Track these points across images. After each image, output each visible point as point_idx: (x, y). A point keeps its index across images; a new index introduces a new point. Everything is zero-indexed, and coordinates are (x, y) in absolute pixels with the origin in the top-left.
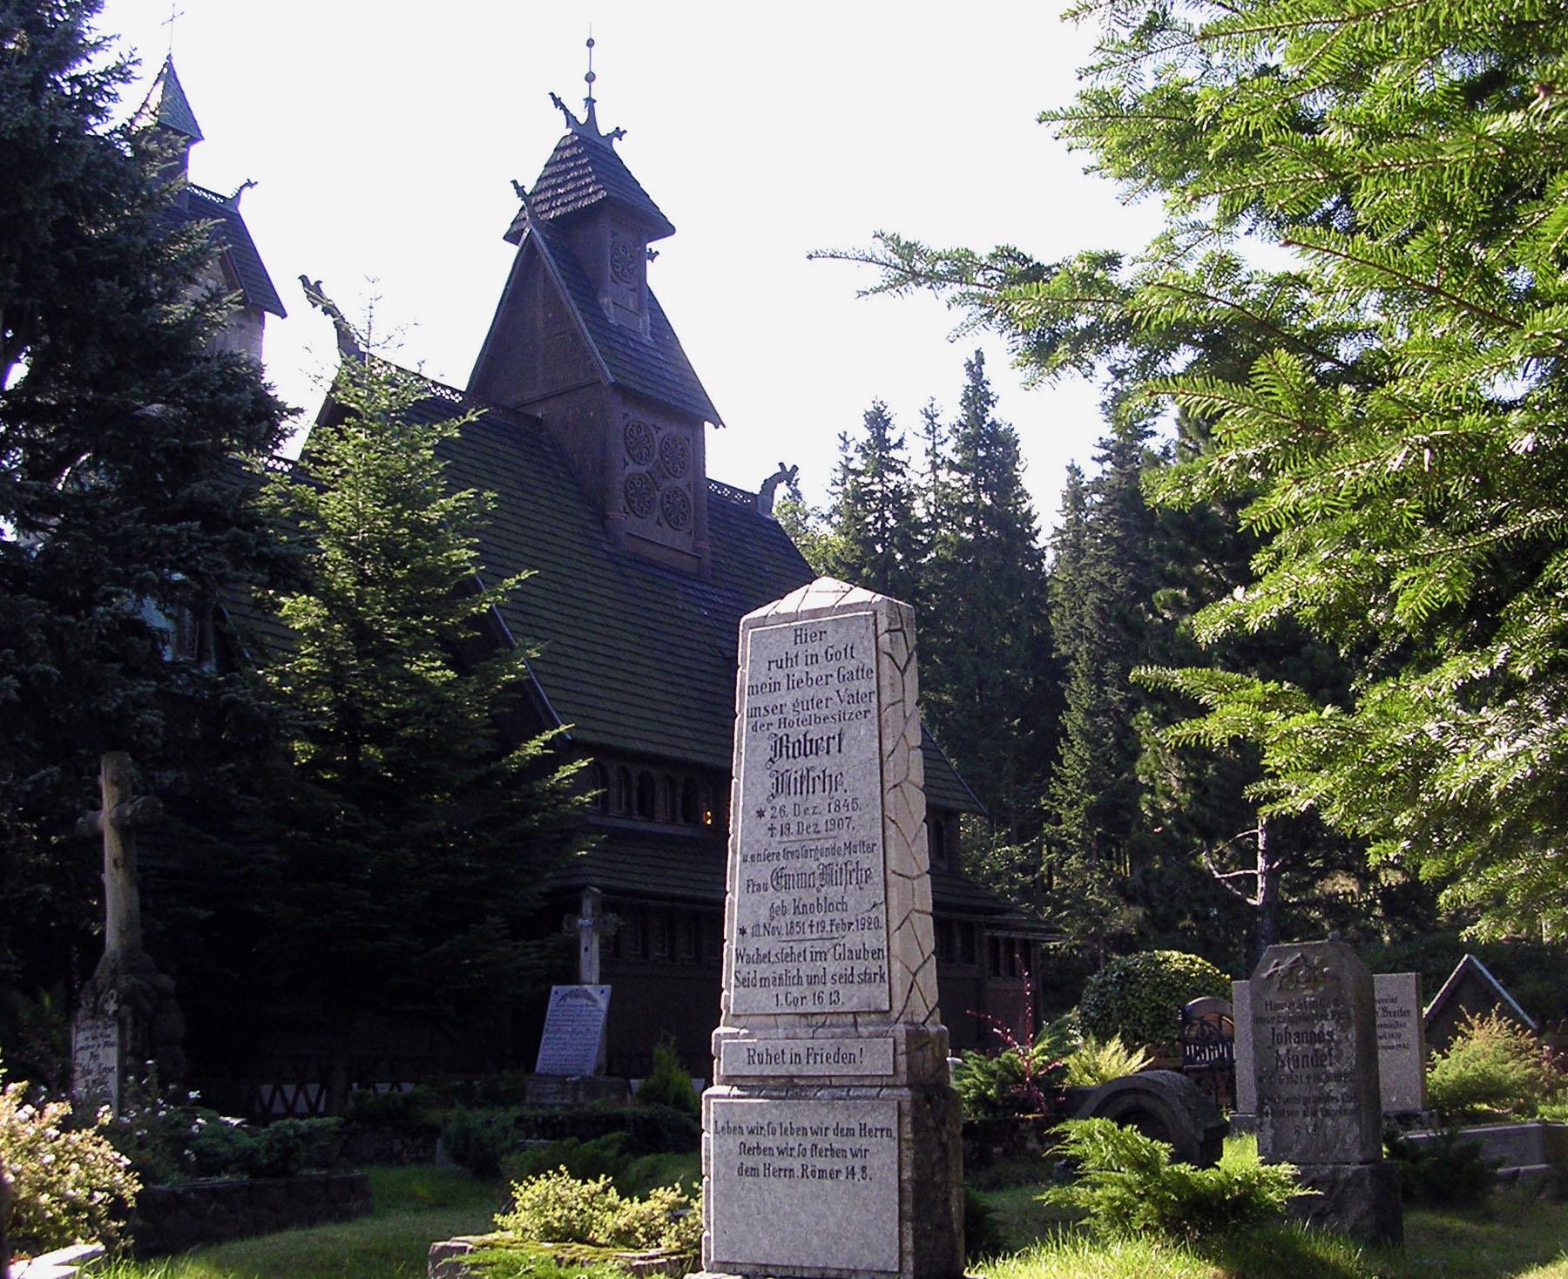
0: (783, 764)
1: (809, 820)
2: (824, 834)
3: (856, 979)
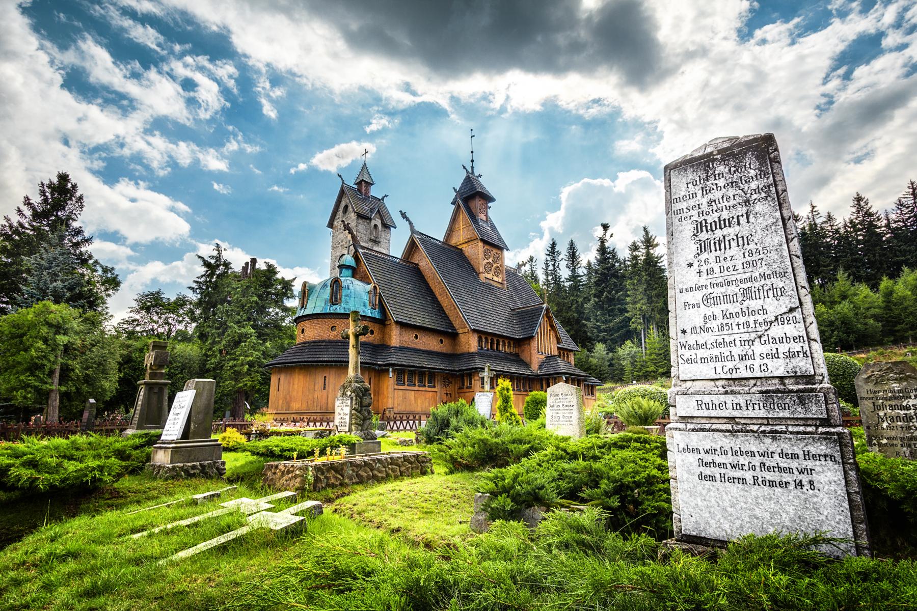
0: (703, 236)
2: (742, 271)
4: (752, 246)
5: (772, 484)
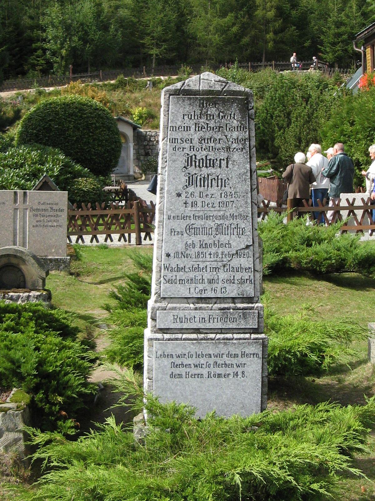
0: (192, 170)
1: (207, 200)
3: (236, 282)
4: (227, 189)
5: (219, 376)
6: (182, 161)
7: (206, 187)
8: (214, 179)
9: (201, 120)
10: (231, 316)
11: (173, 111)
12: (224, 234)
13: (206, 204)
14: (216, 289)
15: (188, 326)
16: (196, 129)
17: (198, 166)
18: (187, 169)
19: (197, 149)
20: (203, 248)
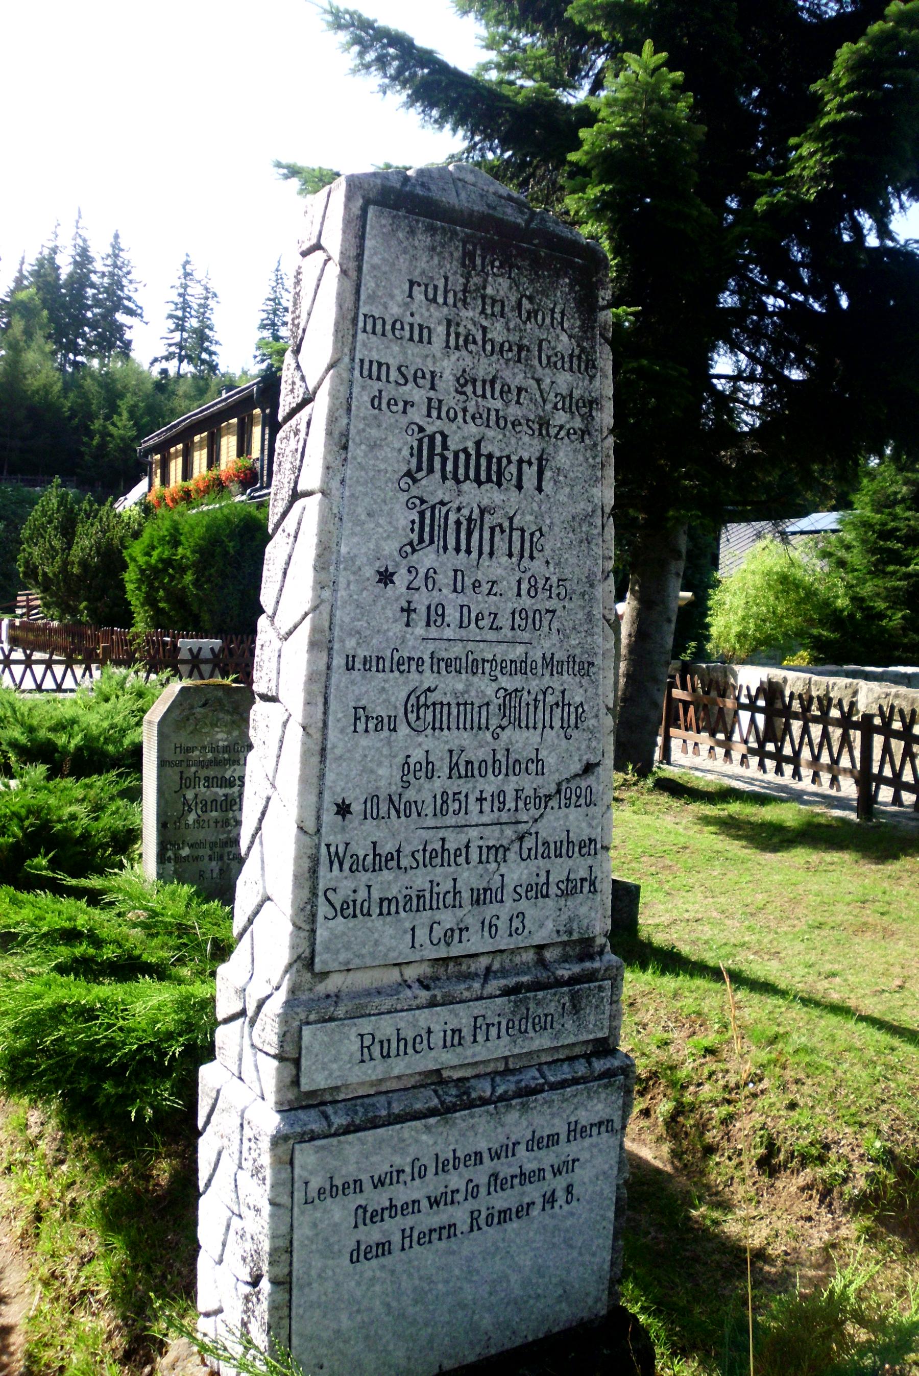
0: (433, 488)
1: (480, 603)
2: (507, 633)
3: (553, 890)
4: (537, 567)
5: (504, 1216)
6: (400, 450)
7: (475, 555)
8: (501, 525)
9: (464, 313)
10: (540, 1011)
11: (376, 260)
12: (523, 724)
13: (473, 616)
14: (494, 921)
15: (408, 1066)
16: (447, 342)
17: (449, 476)
18: (415, 481)
19: (452, 414)
20: (460, 777)
